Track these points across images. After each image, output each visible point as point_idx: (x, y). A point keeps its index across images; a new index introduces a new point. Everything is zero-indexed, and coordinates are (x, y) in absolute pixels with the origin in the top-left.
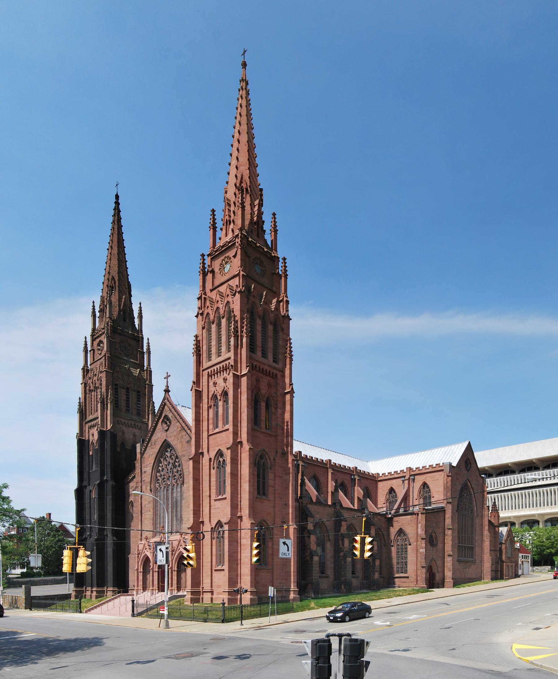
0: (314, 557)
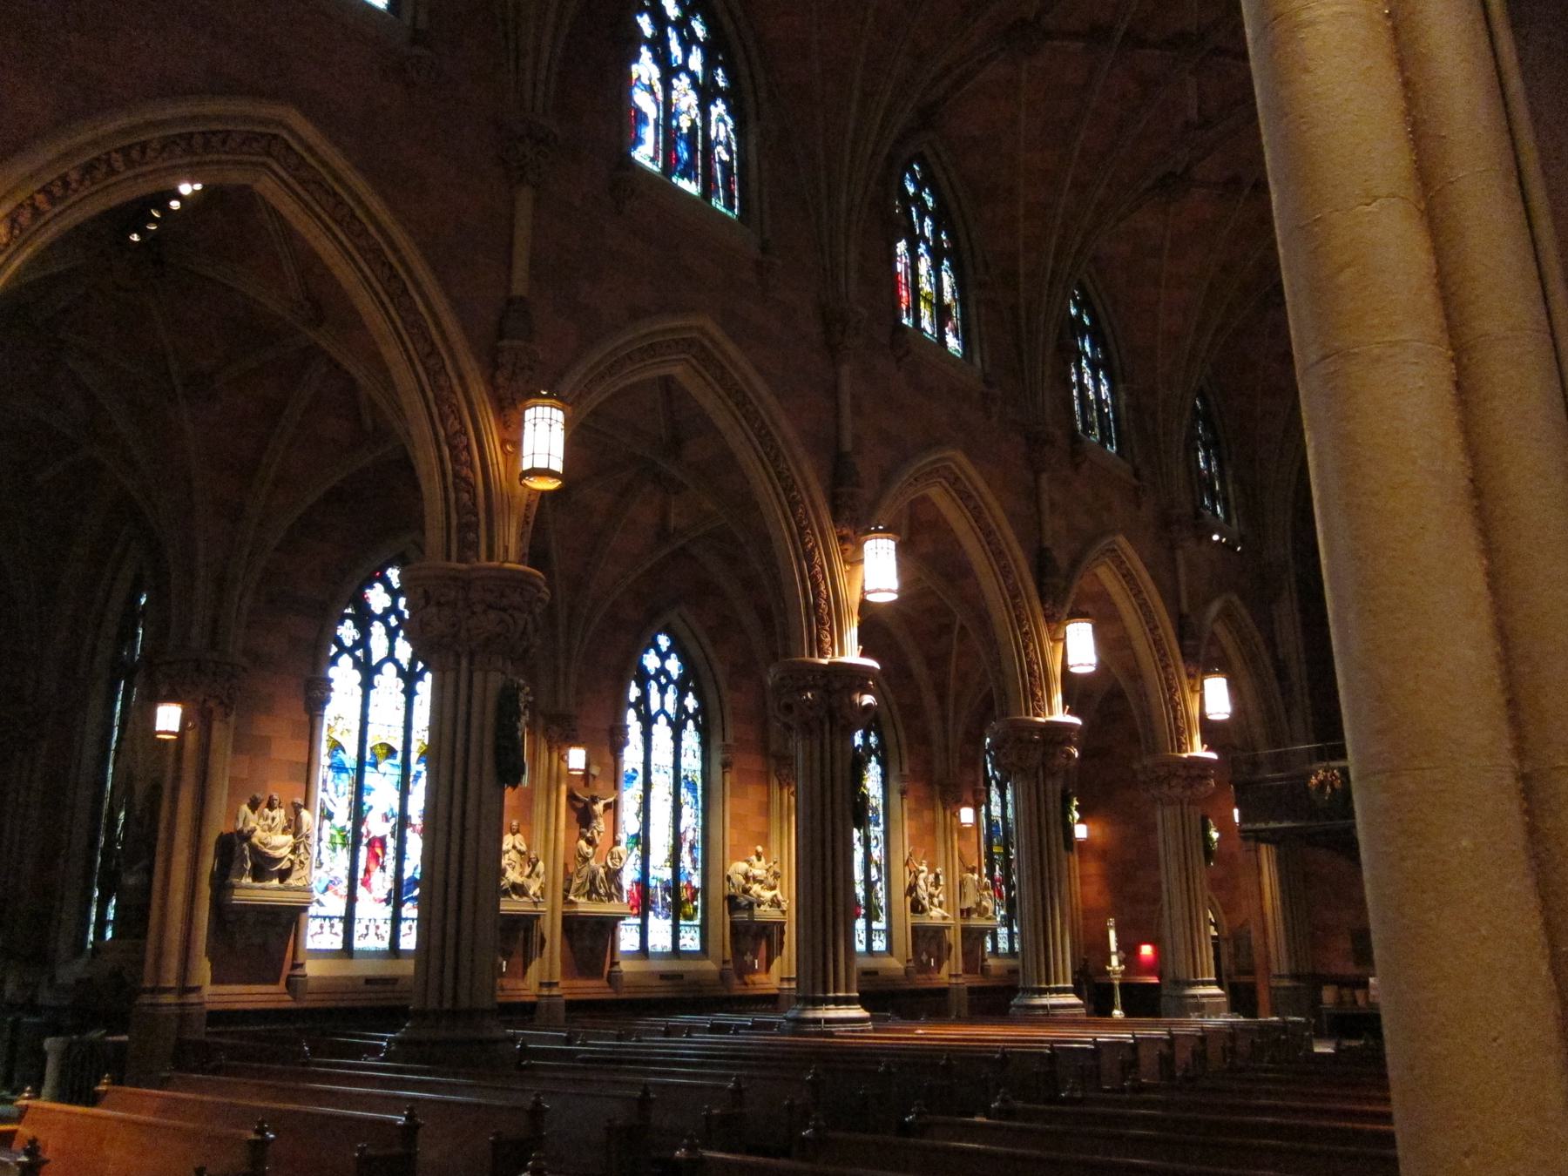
0: (1336, 987)
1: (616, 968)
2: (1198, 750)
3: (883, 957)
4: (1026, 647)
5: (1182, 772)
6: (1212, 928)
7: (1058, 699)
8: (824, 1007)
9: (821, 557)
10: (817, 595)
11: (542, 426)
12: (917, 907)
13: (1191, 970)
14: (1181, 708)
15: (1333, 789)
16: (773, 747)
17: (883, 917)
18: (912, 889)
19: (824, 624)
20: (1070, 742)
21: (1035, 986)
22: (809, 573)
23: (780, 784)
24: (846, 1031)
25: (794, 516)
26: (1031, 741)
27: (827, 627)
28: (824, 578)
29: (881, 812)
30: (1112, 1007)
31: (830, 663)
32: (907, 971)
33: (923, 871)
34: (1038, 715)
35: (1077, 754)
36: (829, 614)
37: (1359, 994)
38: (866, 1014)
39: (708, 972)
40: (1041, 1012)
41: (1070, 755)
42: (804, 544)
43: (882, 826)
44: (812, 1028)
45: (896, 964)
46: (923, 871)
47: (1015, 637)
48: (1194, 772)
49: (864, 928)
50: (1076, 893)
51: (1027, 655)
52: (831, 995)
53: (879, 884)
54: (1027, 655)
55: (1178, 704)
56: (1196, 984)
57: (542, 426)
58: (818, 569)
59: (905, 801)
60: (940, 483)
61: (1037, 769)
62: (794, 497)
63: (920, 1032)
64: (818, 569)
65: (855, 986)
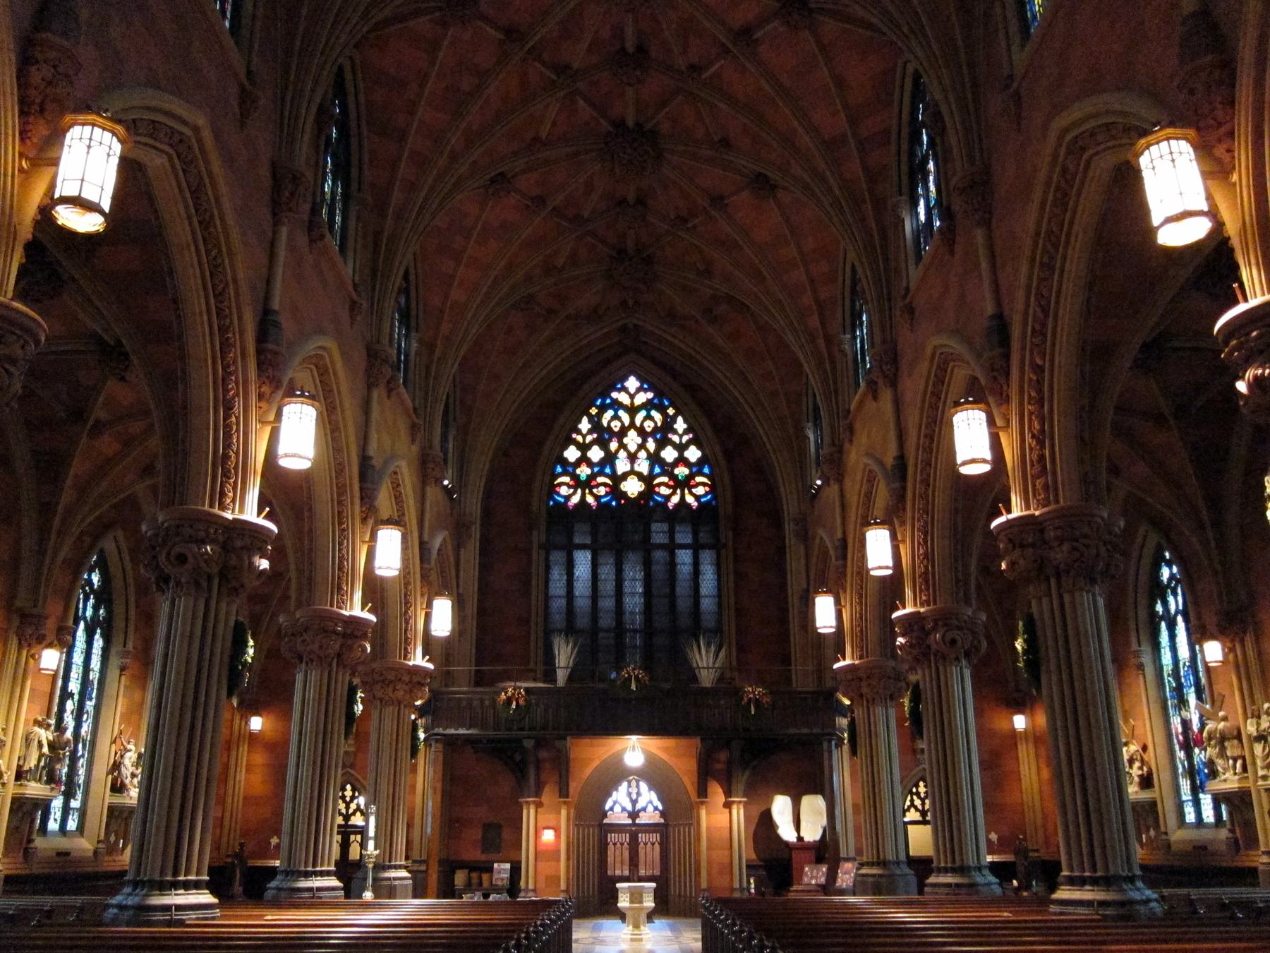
1: (32, 845)
2: (418, 659)
3: (74, 837)
4: (341, 544)
5: (406, 678)
6: (341, 818)
7: (358, 596)
8: (174, 892)
9: (239, 408)
10: (228, 446)
11: (1163, 165)
12: (118, 788)
13: (387, 855)
14: (412, 621)
15: (517, 705)
16: (18, 603)
17: (79, 796)
18: (117, 766)
19: (229, 478)
20: (364, 636)
21: (302, 868)
22: (224, 421)
23: (20, 643)
24: (198, 919)
25: (223, 359)
26: (335, 632)
27: (232, 481)
28: (238, 430)
29: (95, 686)
30: (364, 889)
31: (234, 519)
32: (96, 852)
33: (130, 750)
34: (341, 608)
35: (369, 650)
36: (236, 468)
37: (485, 877)
38: (214, 900)
39: (84, 850)
40: (306, 895)
41: (364, 649)
42: (226, 391)
43: (94, 701)
44: (159, 916)
45: (85, 845)
46: (130, 750)
47: (334, 531)
48: (416, 679)
49: (61, 805)
50: (240, 782)
51: (340, 550)
52: (182, 878)
53: (81, 760)
54: (340, 550)
55: (410, 617)
56: (390, 867)
57: (1163, 165)
58: (234, 419)
59: (123, 678)
60: (311, 371)
61: (333, 659)
62: (228, 339)
63: (269, 918)
64: (234, 419)
65: (206, 869)
